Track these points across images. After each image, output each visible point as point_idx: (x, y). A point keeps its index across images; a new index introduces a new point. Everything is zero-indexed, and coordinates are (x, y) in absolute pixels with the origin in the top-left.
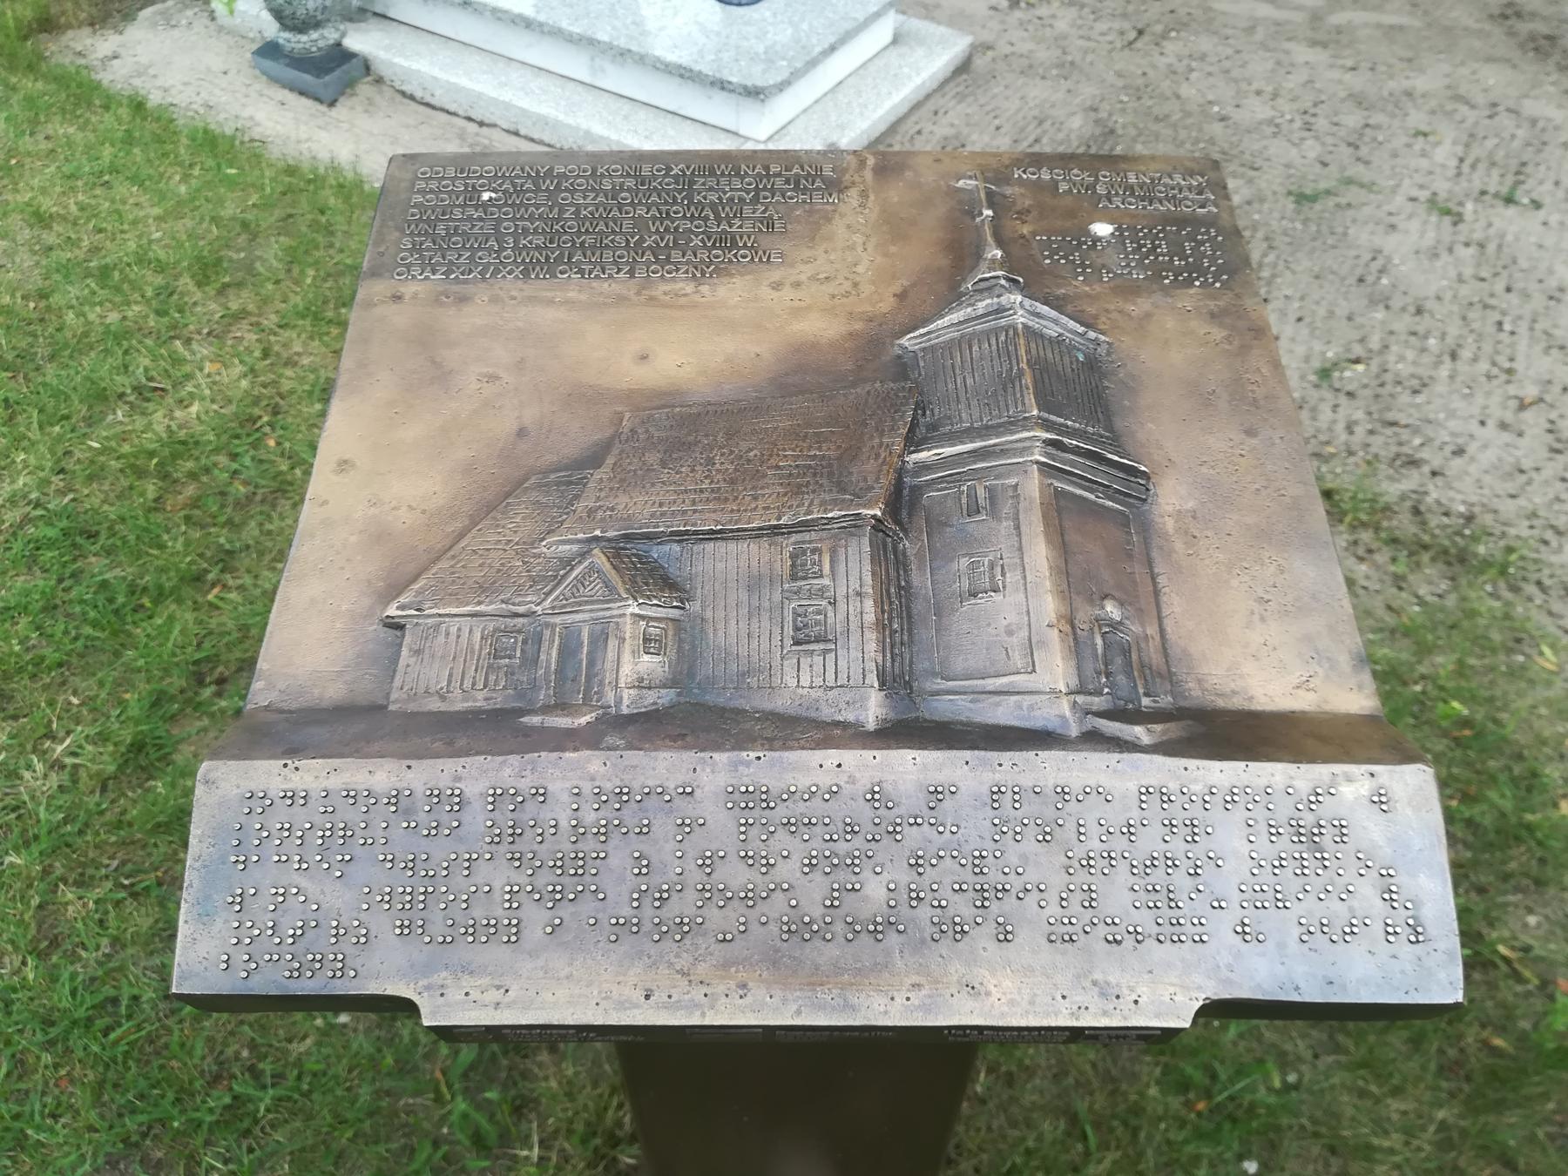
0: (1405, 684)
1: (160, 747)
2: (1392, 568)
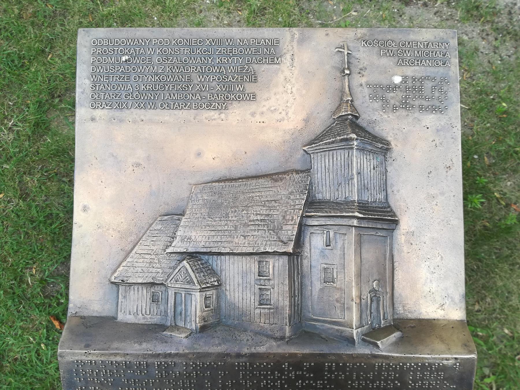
0: (488, 95)
1: (45, 124)
2: (494, 43)
